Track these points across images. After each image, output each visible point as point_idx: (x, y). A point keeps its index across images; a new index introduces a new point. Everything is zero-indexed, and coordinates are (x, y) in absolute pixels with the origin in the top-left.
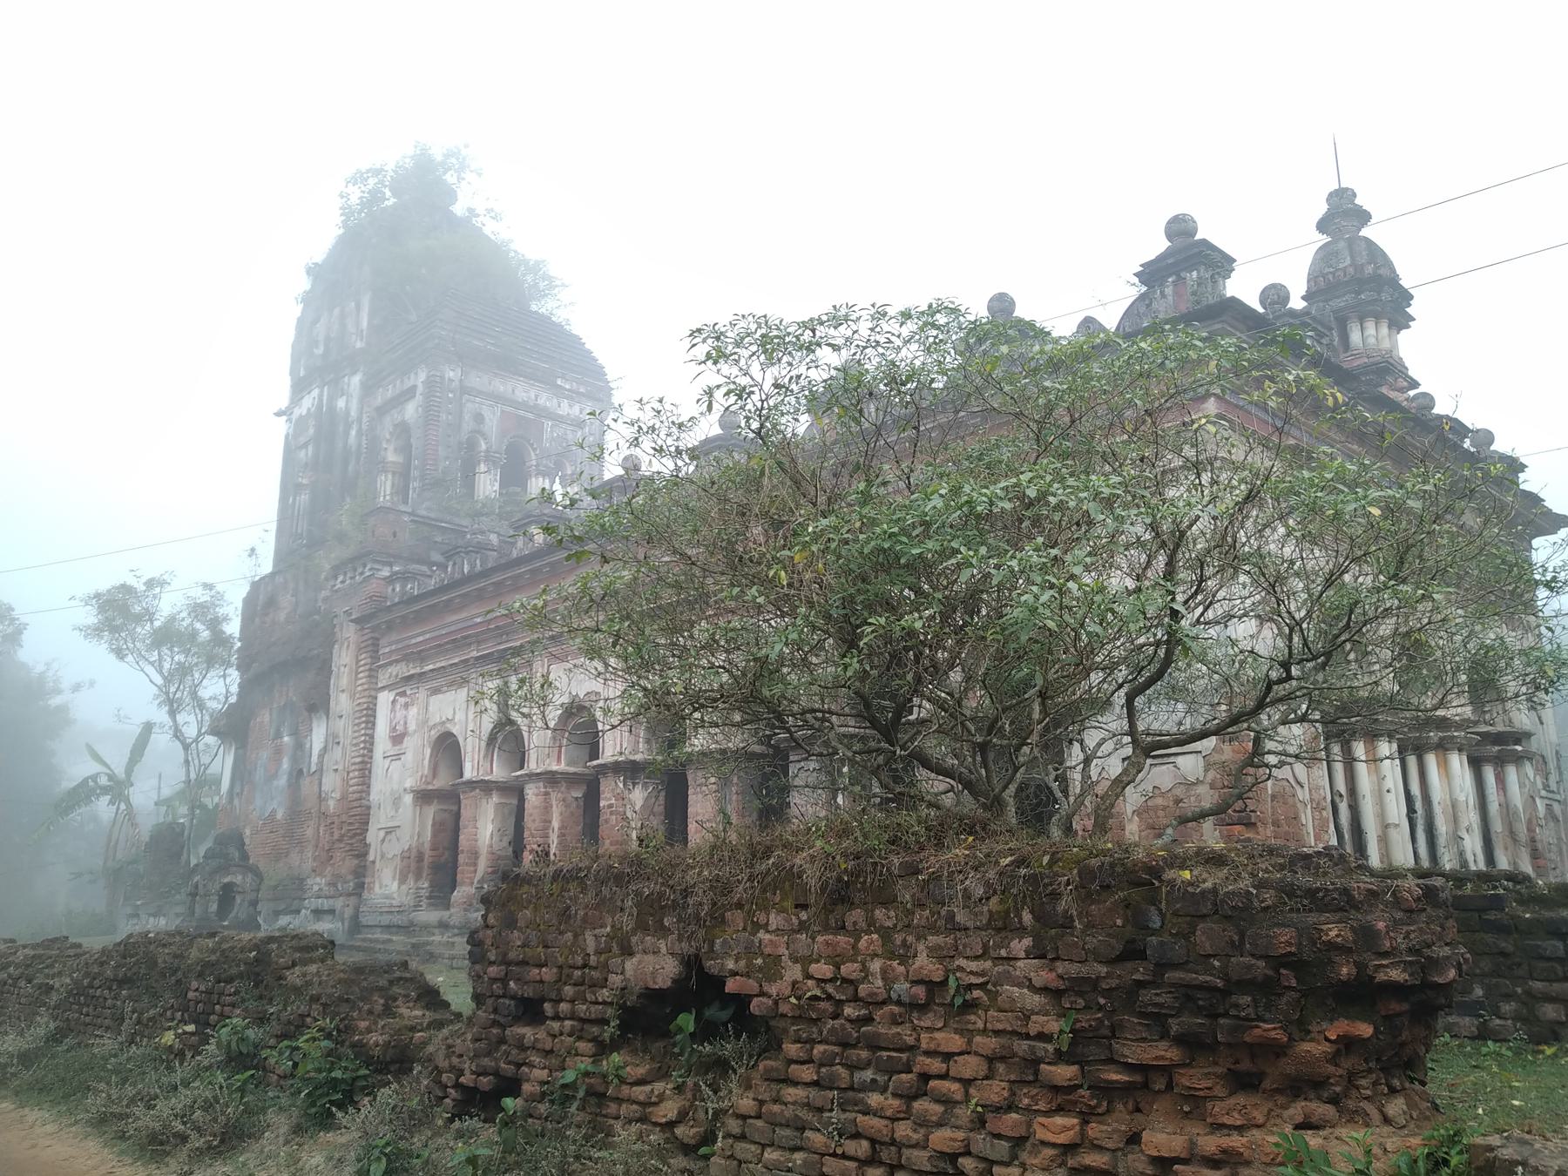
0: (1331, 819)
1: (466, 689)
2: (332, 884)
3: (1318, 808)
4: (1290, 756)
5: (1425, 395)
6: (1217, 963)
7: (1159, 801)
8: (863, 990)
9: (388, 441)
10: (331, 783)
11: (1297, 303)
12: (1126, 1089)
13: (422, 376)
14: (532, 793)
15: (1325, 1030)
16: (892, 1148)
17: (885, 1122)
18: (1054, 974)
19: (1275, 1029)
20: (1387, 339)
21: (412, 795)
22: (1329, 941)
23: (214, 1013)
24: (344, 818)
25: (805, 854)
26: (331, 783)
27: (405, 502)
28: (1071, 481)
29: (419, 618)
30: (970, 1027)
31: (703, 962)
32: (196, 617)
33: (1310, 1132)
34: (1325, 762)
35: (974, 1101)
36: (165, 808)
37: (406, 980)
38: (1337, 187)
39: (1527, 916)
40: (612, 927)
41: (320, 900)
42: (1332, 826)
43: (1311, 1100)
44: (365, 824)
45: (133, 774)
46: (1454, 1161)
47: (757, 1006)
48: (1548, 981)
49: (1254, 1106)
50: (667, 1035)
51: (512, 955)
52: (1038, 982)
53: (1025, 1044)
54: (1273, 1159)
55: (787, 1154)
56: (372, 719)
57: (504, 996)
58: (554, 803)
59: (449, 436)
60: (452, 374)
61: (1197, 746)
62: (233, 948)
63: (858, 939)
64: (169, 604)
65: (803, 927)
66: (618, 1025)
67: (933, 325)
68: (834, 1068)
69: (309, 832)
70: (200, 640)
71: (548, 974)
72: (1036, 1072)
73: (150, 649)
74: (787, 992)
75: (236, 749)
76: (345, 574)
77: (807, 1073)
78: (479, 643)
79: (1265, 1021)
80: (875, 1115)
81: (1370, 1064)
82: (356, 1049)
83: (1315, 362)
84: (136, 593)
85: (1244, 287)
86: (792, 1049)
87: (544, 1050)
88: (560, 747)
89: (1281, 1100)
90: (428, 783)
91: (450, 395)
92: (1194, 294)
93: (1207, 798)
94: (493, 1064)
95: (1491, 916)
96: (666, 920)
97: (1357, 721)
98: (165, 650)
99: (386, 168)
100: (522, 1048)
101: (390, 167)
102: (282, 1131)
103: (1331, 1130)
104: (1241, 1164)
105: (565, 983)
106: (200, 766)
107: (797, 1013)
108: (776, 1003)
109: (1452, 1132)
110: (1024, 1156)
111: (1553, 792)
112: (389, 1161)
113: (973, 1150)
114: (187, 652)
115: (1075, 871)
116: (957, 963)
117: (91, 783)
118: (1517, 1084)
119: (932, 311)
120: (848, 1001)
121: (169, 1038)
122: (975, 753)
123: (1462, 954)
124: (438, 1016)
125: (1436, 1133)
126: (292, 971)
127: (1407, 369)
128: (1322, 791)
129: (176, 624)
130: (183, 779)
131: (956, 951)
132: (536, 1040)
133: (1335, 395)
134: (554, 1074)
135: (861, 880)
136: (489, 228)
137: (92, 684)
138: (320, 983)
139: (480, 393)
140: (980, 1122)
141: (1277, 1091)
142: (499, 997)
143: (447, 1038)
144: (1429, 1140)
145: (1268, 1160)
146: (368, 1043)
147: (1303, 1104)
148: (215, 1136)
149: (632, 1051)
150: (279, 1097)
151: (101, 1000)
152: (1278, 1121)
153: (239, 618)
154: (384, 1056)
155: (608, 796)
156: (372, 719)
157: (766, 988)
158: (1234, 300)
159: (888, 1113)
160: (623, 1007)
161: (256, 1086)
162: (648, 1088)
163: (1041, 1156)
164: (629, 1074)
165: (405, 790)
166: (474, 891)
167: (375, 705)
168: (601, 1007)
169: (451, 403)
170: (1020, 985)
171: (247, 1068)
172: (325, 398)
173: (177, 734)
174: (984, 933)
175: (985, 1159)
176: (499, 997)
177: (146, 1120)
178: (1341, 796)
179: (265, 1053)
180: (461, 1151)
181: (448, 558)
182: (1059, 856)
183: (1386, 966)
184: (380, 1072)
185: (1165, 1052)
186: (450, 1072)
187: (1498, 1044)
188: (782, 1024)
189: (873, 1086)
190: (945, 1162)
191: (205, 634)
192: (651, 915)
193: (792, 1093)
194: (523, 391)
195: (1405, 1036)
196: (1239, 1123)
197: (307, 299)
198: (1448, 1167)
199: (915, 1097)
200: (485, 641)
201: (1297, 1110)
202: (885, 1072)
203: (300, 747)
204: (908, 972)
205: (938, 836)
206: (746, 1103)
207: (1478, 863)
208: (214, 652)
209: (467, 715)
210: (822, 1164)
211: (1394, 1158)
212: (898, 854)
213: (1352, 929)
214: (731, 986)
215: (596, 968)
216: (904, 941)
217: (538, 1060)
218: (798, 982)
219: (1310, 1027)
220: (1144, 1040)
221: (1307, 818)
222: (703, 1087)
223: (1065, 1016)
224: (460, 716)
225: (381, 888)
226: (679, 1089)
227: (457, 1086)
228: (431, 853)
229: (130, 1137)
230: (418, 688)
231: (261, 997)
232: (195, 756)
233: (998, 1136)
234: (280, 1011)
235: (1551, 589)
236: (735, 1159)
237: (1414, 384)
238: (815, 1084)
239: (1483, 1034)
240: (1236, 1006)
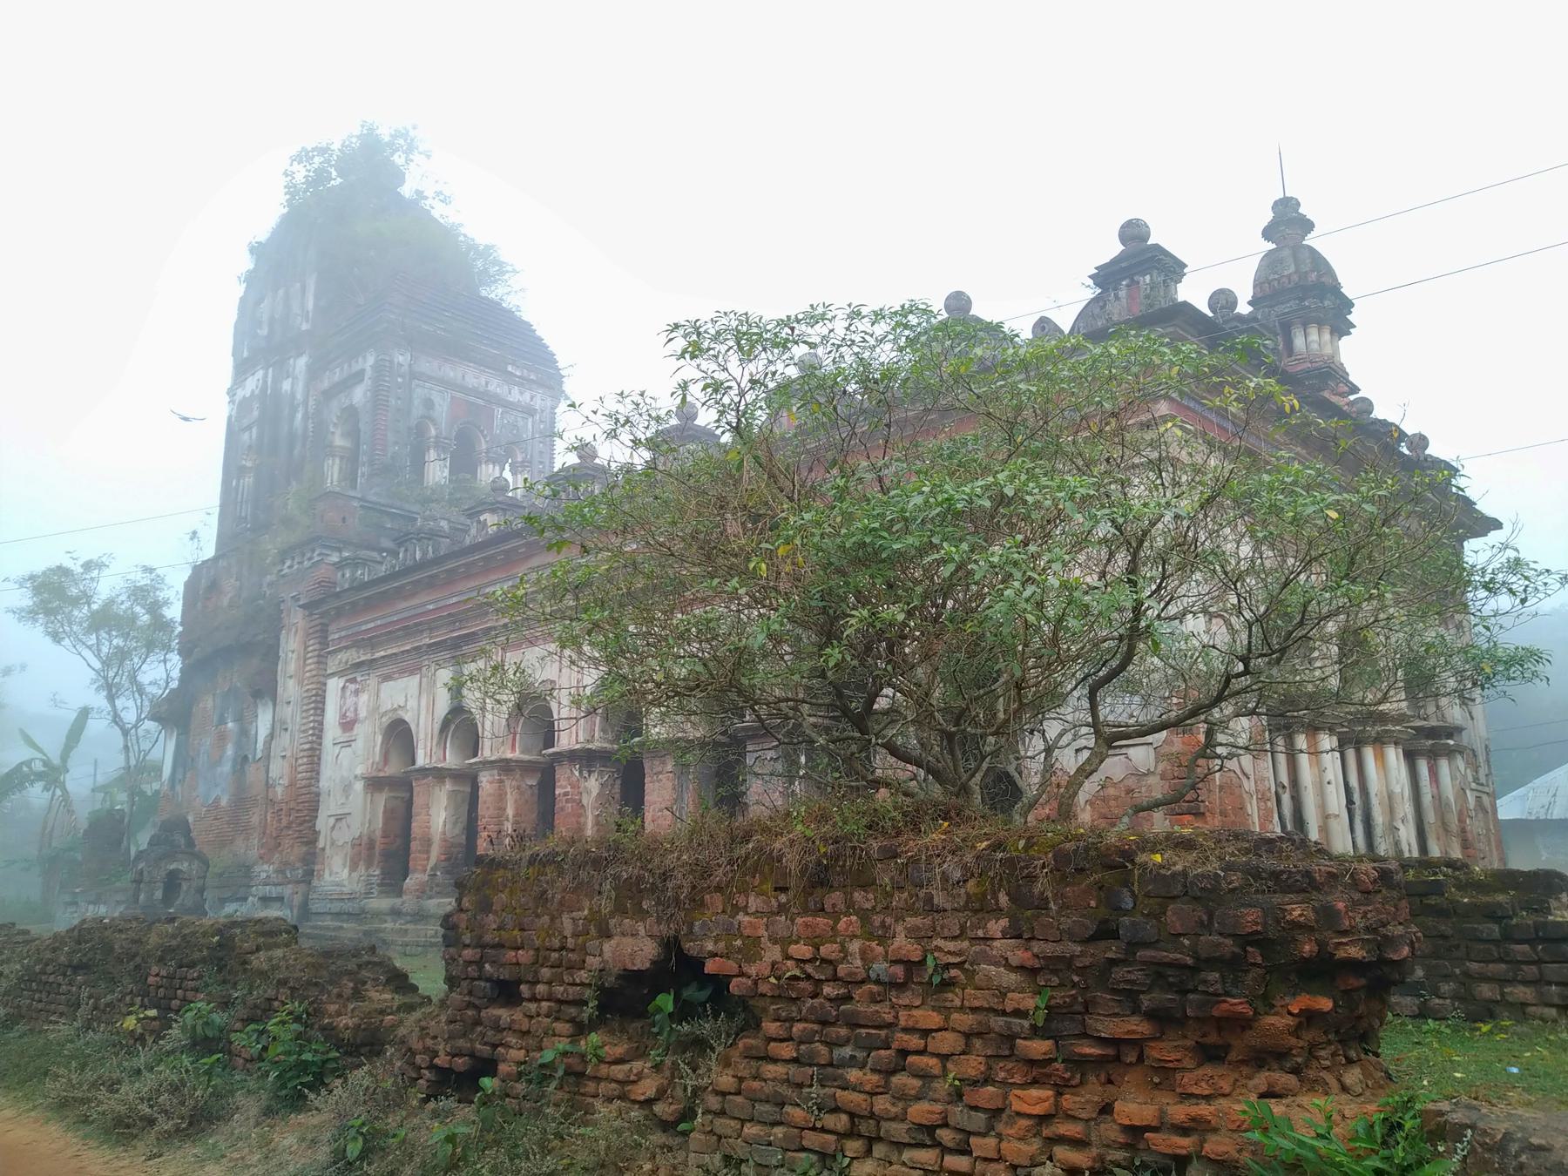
0: (1275, 808)
1: (418, 676)
2: (281, 871)
3: (1263, 798)
4: (1241, 748)
5: (1364, 400)
6: (1186, 942)
7: (1111, 791)
8: (842, 970)
9: (335, 424)
10: (279, 770)
11: (1243, 308)
12: (1100, 1062)
13: (371, 360)
14: (486, 781)
15: (1288, 1005)
16: (871, 1121)
17: (863, 1096)
18: (1030, 953)
19: (1241, 1003)
20: (1329, 345)
21: (362, 782)
22: (1293, 920)
23: (176, 998)
24: (292, 805)
25: (784, 839)
26: (278, 769)
27: (354, 487)
28: (1044, 481)
29: (370, 605)
30: (948, 1004)
31: (682, 943)
32: (136, 600)
33: (1273, 1100)
34: (1269, 754)
35: (951, 1076)
36: (102, 795)
37: (375, 964)
38: (1282, 196)
39: (1466, 900)
40: (590, 909)
41: (268, 887)
42: (1276, 816)
43: (1274, 1071)
44: (314, 809)
45: (69, 760)
46: (1408, 1125)
47: (737, 986)
48: (1484, 962)
49: (1222, 1077)
50: (643, 1014)
51: (488, 938)
52: (1014, 961)
53: (1001, 1020)
54: (1239, 1126)
55: (766, 1128)
56: (320, 705)
57: (479, 978)
58: (508, 790)
59: (399, 421)
60: (402, 358)
61: (1149, 739)
62: (194, 933)
63: (837, 921)
64: (106, 587)
65: (782, 909)
66: (597, 1006)
67: (906, 326)
68: (813, 1046)
69: (255, 820)
70: (139, 623)
71: (524, 956)
72: (1012, 1047)
73: (88, 631)
74: (767, 972)
75: (178, 735)
76: (293, 559)
77: (787, 1050)
78: (431, 630)
79: (1233, 996)
80: (854, 1090)
81: (1330, 1037)
82: (326, 1032)
83: (1272, 371)
84: (73, 575)
85: (1194, 292)
86: (771, 1027)
87: (521, 1031)
88: (515, 734)
89: (1246, 1070)
90: (380, 770)
91: (400, 380)
92: (1147, 297)
93: (1157, 788)
94: (469, 1045)
95: (1432, 900)
96: (644, 903)
97: (1305, 715)
98: (103, 634)
99: (332, 147)
100: (498, 1028)
101: (336, 146)
102: (251, 1114)
103: (1293, 1099)
104: (1208, 1131)
105: (542, 966)
106: (140, 752)
107: (776, 993)
108: (756, 983)
109: (1406, 1099)
110: (1000, 1127)
111: (1482, 785)
112: (365, 1141)
113: (951, 1122)
114: (126, 636)
115: (1050, 855)
116: (935, 943)
117: (25, 769)
118: (1456, 1058)
119: (905, 311)
120: (827, 980)
121: (130, 1023)
122: (942, 740)
123: (1414, 933)
124: (407, 999)
125: (1390, 1100)
126: (257, 955)
127: (1348, 374)
128: (1266, 782)
129: (115, 607)
130: (123, 765)
131: (933, 932)
132: (513, 1021)
133: (1290, 401)
134: (531, 1054)
135: (841, 863)
136: (438, 211)
137: (23, 667)
138: (287, 968)
139: (430, 378)
140: (958, 1095)
141: (1242, 1062)
142: (474, 979)
143: (420, 1020)
144: (1384, 1107)
145: (1234, 1127)
146: (338, 1025)
147: (1267, 1074)
148: (183, 1118)
149: (609, 1032)
150: (246, 1080)
151: (54, 985)
152: (1244, 1091)
153: (181, 602)
154: (354, 1038)
155: (564, 783)
156: (320, 705)
157: (745, 969)
158: (1185, 304)
159: (868, 1088)
160: (601, 988)
161: (223, 1070)
162: (626, 1067)
163: (1017, 1127)
164: (607, 1053)
165: (356, 777)
166: (426, 878)
167: (325, 691)
168: (578, 988)
169: (400, 388)
170: (997, 964)
171: (212, 1053)
172: (270, 380)
173: (116, 719)
174: (961, 914)
175: (962, 1131)
176: (474, 979)
177: (112, 1104)
178: (1284, 787)
179: (233, 1037)
180: (438, 1131)
181: (400, 545)
182: (1035, 840)
183: (1346, 944)
184: (350, 1054)
185: (1136, 1026)
186: (424, 1053)
187: (1437, 1023)
188: (761, 1003)
189: (852, 1062)
190: (923, 1133)
191: (145, 618)
192: (630, 897)
193: (771, 1070)
194: (474, 378)
195: (1362, 1009)
196: (1206, 1092)
197: (250, 279)
198: (1403, 1131)
199: (894, 1072)
200: (437, 628)
201: (1261, 1080)
202: (863, 1048)
203: (245, 733)
204: (887, 952)
205: (914, 820)
206: (726, 1081)
207: (1410, 848)
208: (155, 636)
209: (419, 701)
210: (801, 1138)
211: (1352, 1124)
212: (876, 838)
213: (1314, 909)
214: (710, 967)
215: (573, 950)
216: (883, 922)
217: (514, 1041)
218: (777, 963)
219: (1274, 1002)
220: (1116, 1015)
221: (1253, 808)
222: (682, 1065)
223: (1040, 993)
224: (412, 703)
225: (330, 875)
226: (657, 1067)
227: (432, 1067)
228: (383, 840)
229: (93, 1122)
230: (369, 674)
231: (224, 982)
232: (134, 742)
233: (976, 1108)
234: (245, 995)
235: (1489, 590)
236: (715, 1134)
237: (1354, 389)
238: (795, 1061)
239: (1423, 1014)
240: (1205, 982)
